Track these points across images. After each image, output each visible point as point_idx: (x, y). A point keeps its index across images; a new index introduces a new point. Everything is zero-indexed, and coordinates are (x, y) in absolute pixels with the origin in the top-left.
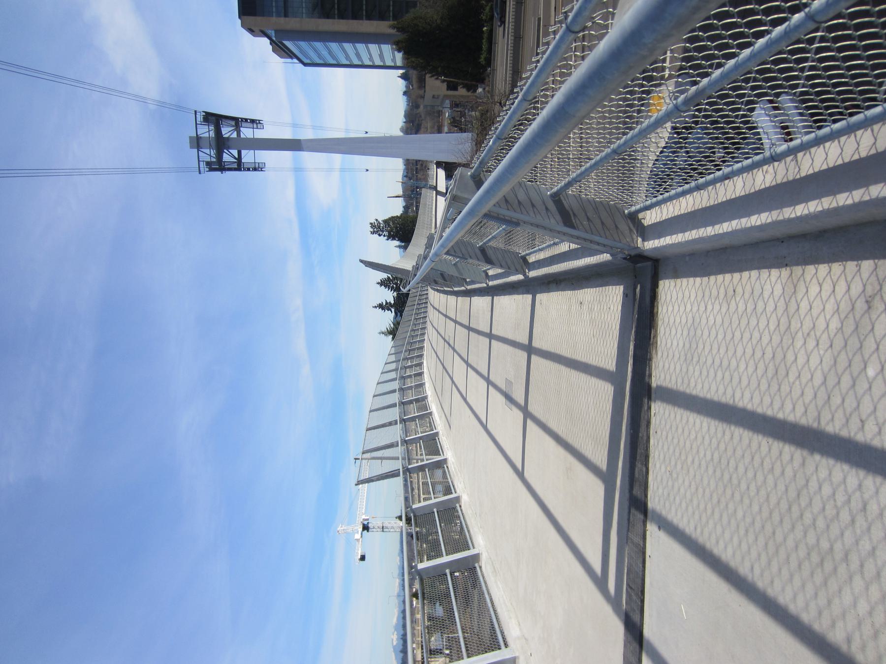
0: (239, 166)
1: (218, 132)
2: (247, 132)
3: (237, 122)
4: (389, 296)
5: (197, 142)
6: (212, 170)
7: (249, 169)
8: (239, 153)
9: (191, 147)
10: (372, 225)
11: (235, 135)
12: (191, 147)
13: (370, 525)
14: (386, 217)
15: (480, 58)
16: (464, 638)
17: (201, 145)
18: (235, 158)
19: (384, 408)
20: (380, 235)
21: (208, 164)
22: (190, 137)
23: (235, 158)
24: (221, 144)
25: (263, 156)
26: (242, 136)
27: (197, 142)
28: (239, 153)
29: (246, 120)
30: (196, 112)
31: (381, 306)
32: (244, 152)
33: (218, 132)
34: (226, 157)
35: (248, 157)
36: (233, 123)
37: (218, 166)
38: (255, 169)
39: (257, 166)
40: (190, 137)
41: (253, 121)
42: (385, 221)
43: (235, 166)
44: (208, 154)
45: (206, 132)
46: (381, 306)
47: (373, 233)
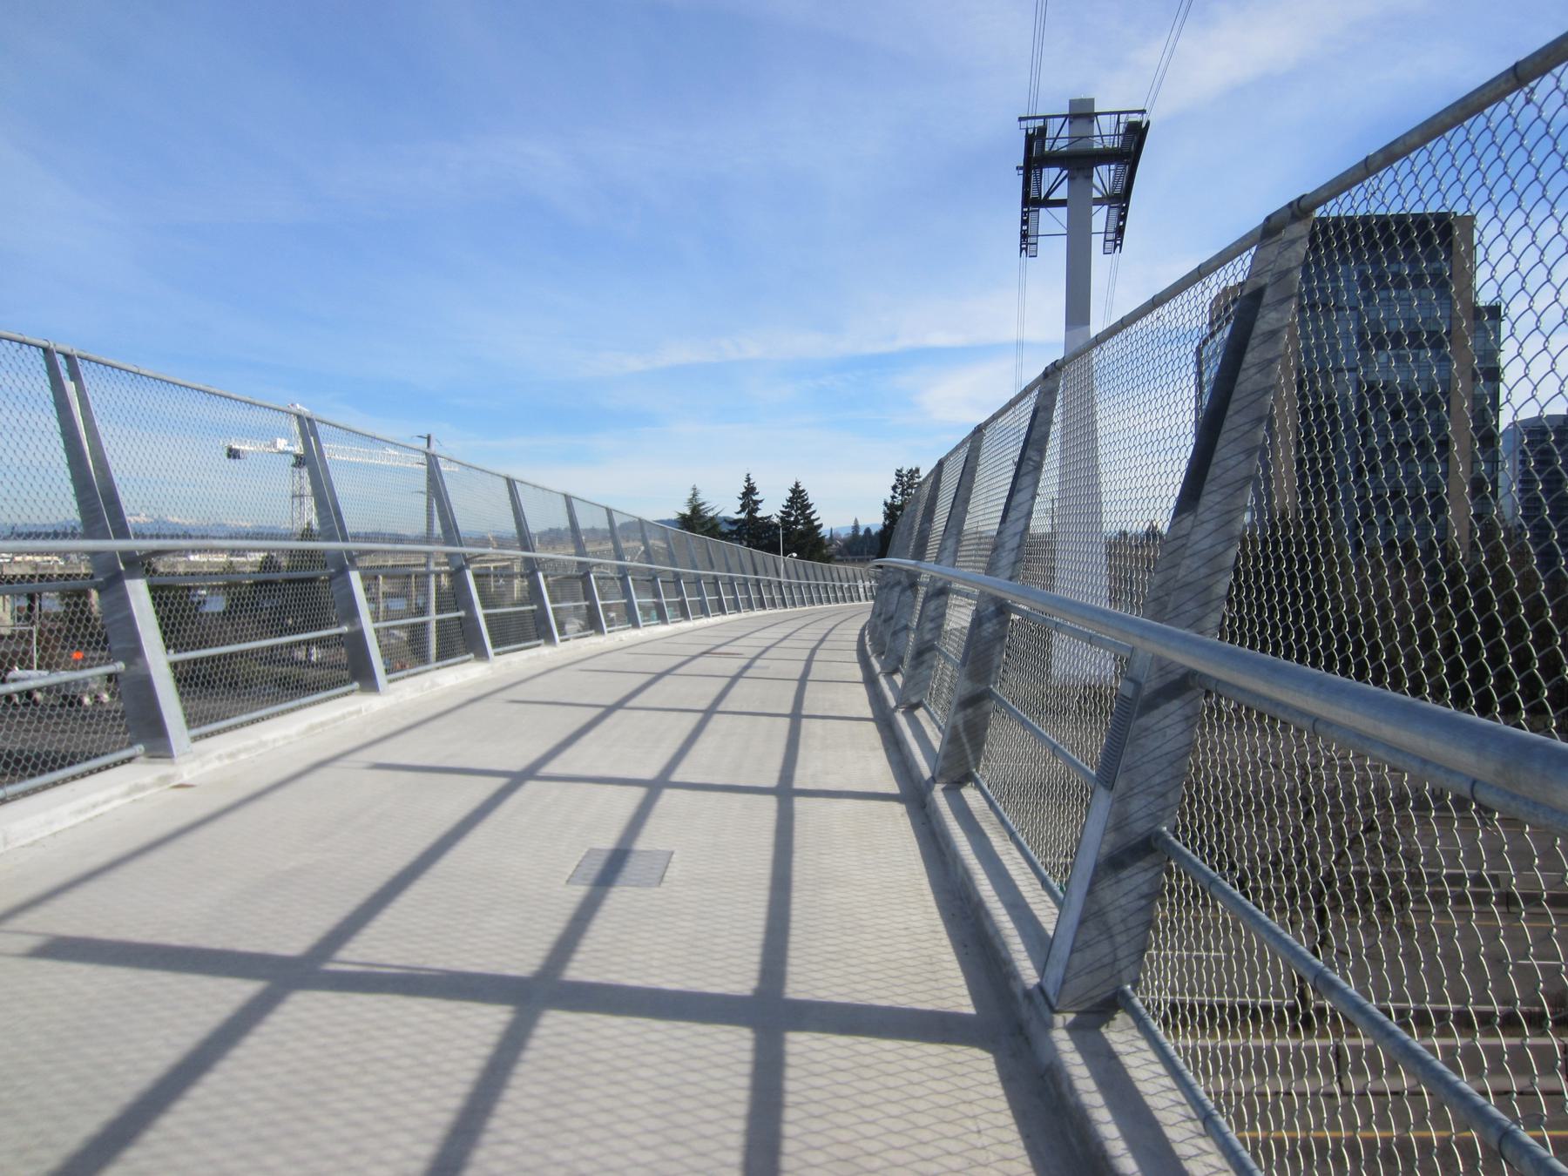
0: (1032, 202)
5: (1082, 113)
7: (1024, 222)
9: (1071, 102)
18: (1049, 193)
20: (894, 488)
22: (1092, 101)
23: (1049, 193)
24: (1079, 162)
26: (1095, 208)
29: (1123, 218)
31: (750, 491)
32: (1061, 213)
35: (1052, 221)
39: (1031, 240)
40: (1092, 101)
41: (1120, 232)
44: (1060, 138)
45: (1106, 132)
46: (750, 491)
47: (899, 474)
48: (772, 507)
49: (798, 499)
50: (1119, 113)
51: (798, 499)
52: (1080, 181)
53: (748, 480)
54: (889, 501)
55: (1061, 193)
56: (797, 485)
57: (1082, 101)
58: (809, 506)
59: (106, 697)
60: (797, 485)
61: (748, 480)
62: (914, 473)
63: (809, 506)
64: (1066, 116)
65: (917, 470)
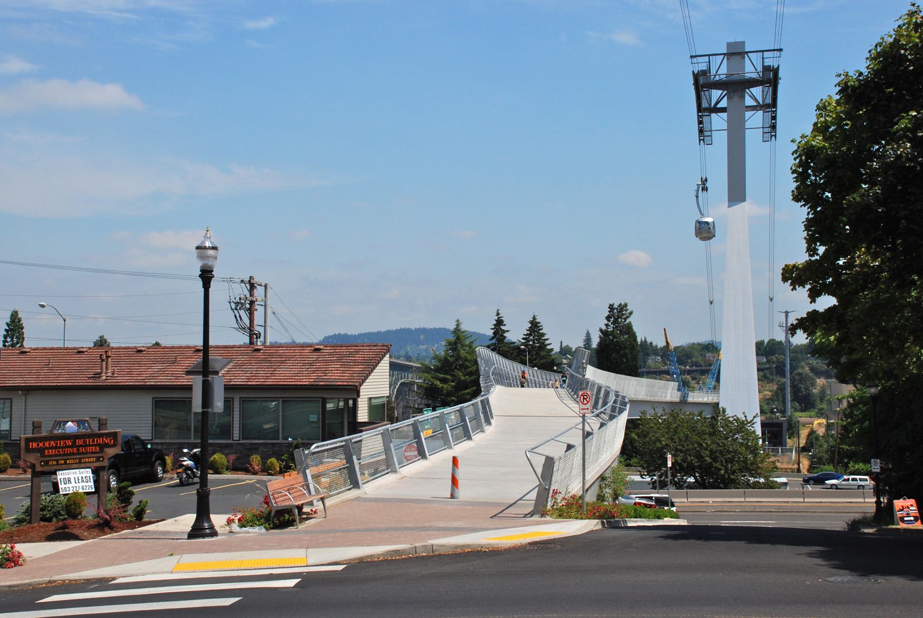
0: (704, 110)
1: (753, 83)
2: (755, 120)
3: (770, 106)
4: (516, 334)
5: (736, 53)
6: (696, 77)
7: (700, 122)
8: (723, 110)
9: (729, 44)
10: (623, 307)
11: (749, 102)
12: (729, 44)
13: (410, 354)
14: (635, 328)
15: (856, 462)
16: (784, 402)
17: (733, 58)
18: (717, 103)
19: (111, 272)
20: (608, 318)
21: (704, 73)
22: (743, 43)
23: (717, 103)
24: (736, 86)
25: (720, 139)
26: (748, 114)
27: (736, 53)
28: (723, 110)
29: (774, 118)
30: (781, 50)
31: (499, 322)
32: (724, 115)
33: (753, 83)
34: (716, 94)
35: (718, 121)
36: (769, 100)
37: (702, 83)
38: (701, 131)
39: (706, 134)
40: (743, 43)
41: (773, 127)
42: (629, 327)
43: (705, 105)
44: (721, 70)
45: (751, 69)
46: (499, 322)
47: (611, 307)
48: (516, 334)
49: (535, 326)
50: (763, 51)
51: (535, 326)
52: (736, 99)
53: (498, 314)
54: (604, 328)
55: (723, 104)
56: (534, 318)
57: (736, 43)
58: (543, 335)
59: (902, 52)
60: (534, 318)
61: (498, 314)
62: (763, 342)
63: (543, 335)
64: (725, 54)
65: (626, 305)
